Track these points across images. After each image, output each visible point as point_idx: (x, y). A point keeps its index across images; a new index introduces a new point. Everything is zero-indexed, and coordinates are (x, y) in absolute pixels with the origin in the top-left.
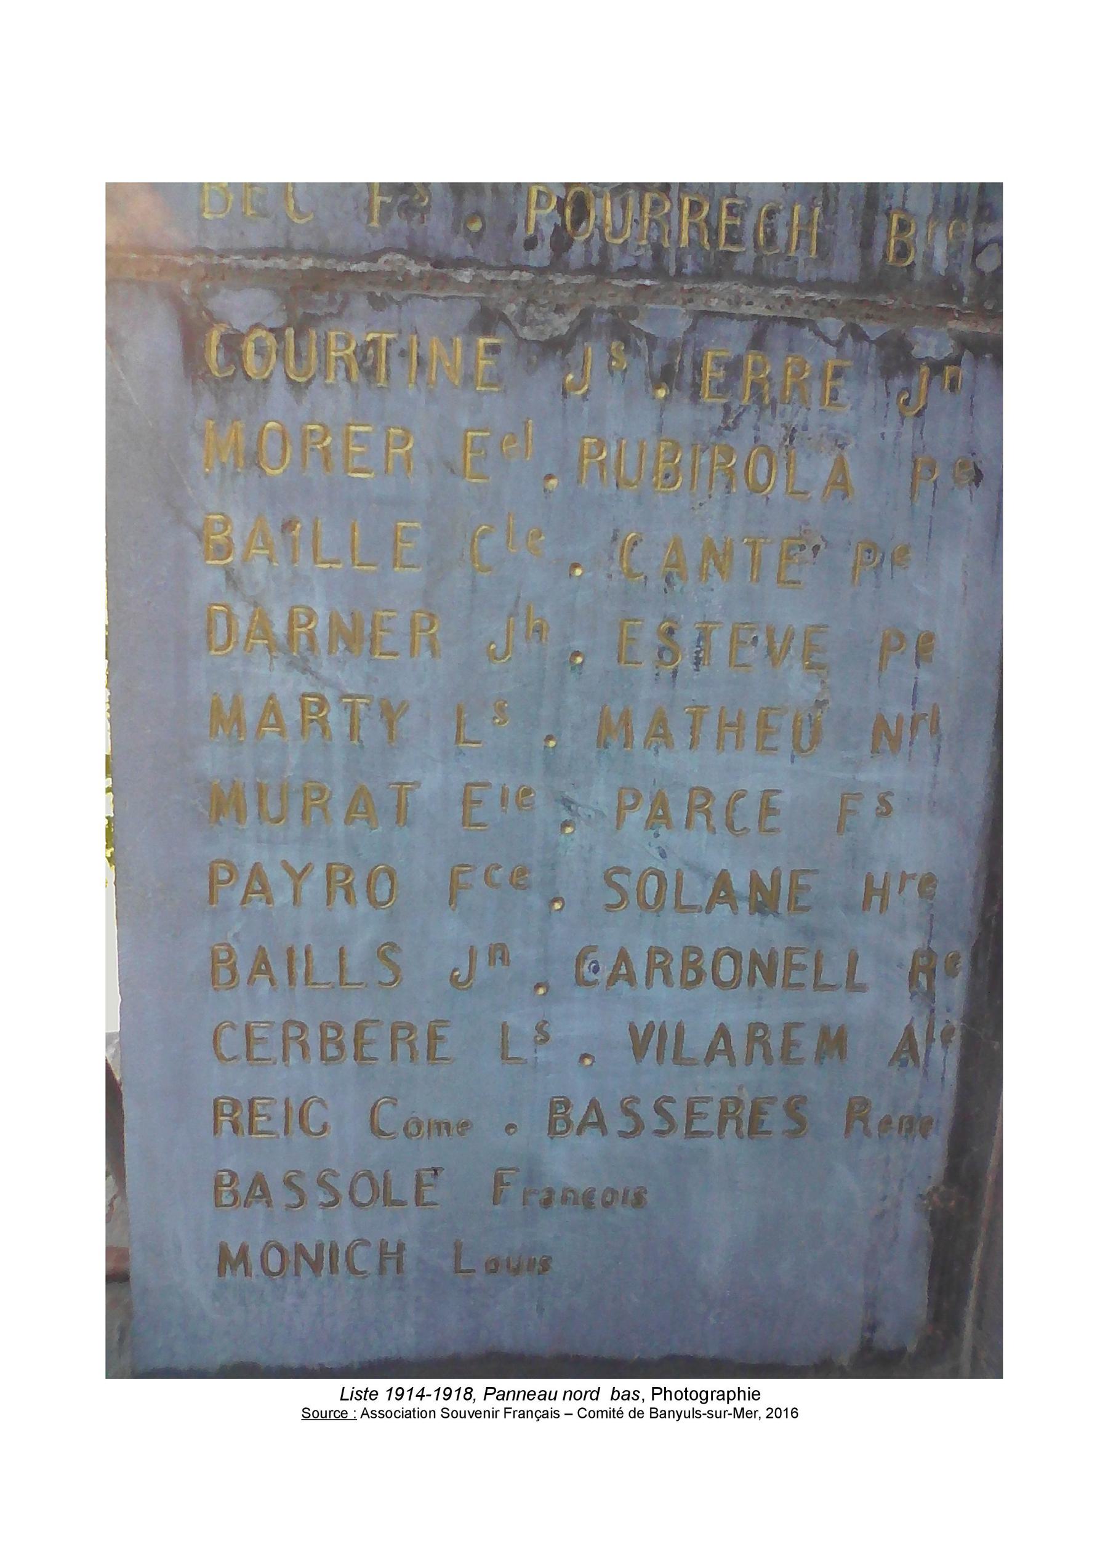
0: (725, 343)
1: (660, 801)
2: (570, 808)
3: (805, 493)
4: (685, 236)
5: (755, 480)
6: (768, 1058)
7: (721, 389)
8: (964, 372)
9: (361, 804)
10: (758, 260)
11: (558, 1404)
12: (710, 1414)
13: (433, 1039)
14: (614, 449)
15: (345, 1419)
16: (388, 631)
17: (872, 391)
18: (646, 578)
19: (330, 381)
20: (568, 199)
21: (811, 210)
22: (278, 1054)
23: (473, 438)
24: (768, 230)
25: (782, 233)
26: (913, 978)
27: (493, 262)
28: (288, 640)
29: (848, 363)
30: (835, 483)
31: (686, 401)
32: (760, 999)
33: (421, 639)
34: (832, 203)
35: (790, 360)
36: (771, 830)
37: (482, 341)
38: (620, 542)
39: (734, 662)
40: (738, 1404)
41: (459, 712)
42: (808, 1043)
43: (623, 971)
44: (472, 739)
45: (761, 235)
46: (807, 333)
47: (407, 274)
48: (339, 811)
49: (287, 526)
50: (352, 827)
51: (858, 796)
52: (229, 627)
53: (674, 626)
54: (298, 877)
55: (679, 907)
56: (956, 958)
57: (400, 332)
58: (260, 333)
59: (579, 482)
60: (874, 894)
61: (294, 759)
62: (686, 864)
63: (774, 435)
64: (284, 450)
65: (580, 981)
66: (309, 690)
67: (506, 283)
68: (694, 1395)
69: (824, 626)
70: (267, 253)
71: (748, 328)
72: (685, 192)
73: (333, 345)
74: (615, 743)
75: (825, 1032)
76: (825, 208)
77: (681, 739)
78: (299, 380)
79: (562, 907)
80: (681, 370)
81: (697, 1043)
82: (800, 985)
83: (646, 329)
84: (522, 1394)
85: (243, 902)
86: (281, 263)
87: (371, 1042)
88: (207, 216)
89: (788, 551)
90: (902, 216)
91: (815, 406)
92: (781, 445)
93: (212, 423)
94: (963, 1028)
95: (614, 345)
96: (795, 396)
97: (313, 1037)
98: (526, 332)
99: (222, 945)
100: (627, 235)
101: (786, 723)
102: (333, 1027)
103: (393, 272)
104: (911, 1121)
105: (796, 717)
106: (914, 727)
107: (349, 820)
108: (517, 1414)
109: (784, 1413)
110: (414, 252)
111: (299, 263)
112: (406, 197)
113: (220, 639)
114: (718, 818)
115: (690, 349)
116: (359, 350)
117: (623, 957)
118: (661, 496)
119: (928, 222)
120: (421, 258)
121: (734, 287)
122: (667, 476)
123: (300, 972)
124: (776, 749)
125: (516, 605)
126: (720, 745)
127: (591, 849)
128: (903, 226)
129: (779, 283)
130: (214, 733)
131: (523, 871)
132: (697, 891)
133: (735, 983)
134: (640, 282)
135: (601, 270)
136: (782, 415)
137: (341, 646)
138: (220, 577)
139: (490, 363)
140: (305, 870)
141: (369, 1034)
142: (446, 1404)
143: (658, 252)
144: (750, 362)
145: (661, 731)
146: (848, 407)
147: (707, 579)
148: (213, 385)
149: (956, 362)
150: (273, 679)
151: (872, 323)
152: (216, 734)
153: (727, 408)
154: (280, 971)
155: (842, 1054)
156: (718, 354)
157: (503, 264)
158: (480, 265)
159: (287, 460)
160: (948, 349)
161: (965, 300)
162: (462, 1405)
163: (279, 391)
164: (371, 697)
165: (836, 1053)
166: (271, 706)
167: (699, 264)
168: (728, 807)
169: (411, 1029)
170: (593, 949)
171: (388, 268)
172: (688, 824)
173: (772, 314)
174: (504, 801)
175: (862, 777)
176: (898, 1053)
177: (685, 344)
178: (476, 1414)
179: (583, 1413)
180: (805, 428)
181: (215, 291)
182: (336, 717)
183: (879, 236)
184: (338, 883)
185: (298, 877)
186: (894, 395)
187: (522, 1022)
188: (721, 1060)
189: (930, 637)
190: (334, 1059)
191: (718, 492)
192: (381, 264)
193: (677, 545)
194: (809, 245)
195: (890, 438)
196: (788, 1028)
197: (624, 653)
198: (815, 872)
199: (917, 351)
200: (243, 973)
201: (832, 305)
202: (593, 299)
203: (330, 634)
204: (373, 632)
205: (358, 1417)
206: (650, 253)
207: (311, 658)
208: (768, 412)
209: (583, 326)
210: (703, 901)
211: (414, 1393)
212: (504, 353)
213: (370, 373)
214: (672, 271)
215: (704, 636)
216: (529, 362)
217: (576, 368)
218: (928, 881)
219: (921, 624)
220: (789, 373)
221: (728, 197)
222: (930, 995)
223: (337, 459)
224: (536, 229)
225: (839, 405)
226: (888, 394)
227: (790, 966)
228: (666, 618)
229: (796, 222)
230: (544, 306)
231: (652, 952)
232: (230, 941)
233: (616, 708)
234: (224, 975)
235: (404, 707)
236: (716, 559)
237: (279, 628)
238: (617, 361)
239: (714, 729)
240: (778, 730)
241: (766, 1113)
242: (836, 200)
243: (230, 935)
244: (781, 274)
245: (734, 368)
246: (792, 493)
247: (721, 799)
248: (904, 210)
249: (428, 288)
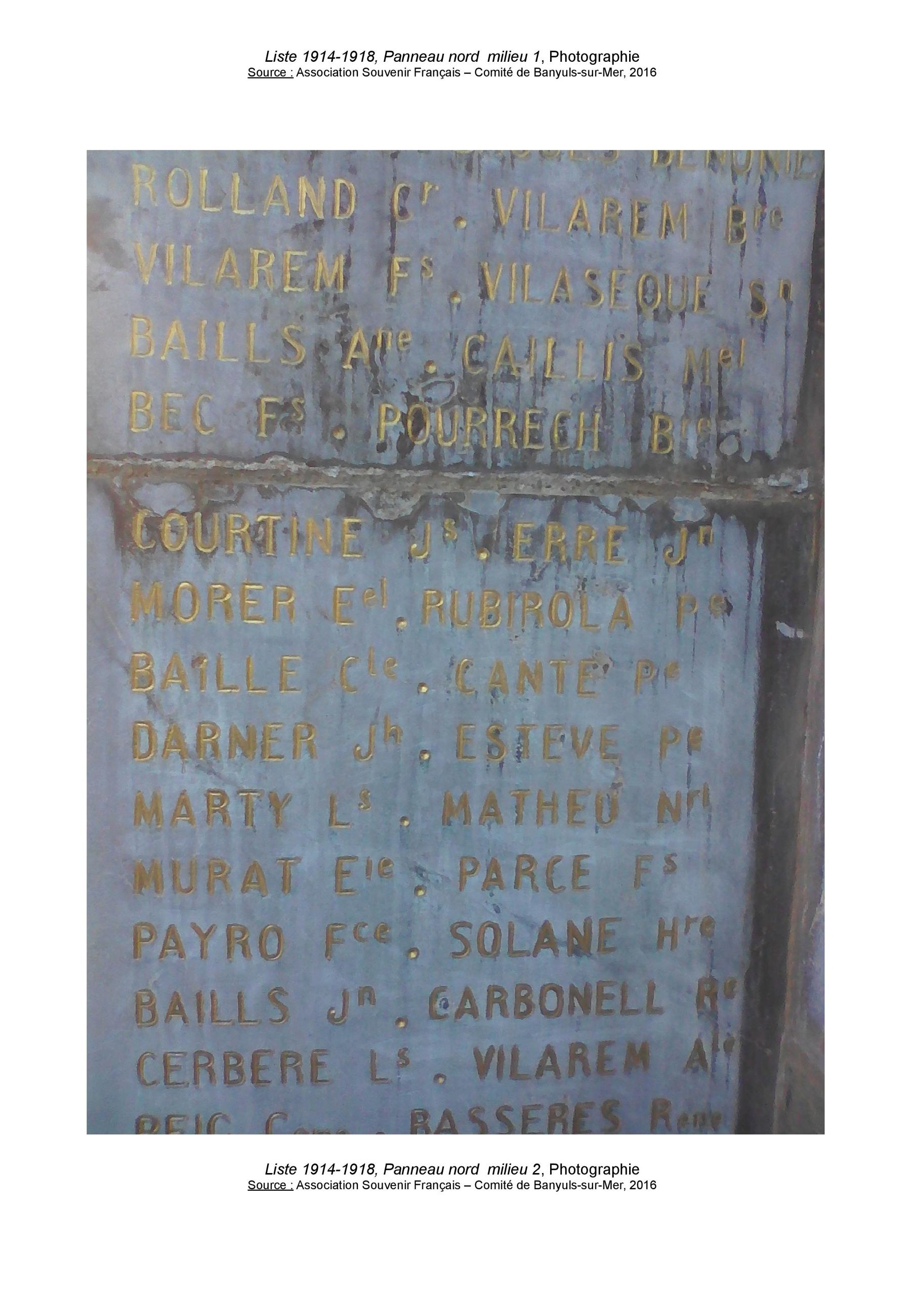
0: (532, 517)
1: (493, 867)
2: (421, 875)
3: (596, 626)
4: (498, 438)
5: (557, 617)
6: (586, 1070)
7: (528, 552)
8: (715, 529)
9: (253, 876)
10: (554, 455)
13: (316, 1064)
14: (449, 598)
15: (283, 1190)
16: (276, 739)
17: (644, 548)
18: (476, 692)
19: (229, 552)
20: (410, 414)
21: (593, 416)
22: (189, 1078)
23: (341, 592)
24: (561, 431)
25: (571, 433)
26: (699, 1002)
27: (354, 462)
28: (197, 751)
29: (624, 528)
30: (619, 618)
31: (503, 561)
32: (579, 1023)
33: (303, 745)
34: (609, 410)
35: (580, 528)
36: (583, 887)
37: (347, 521)
38: (456, 665)
39: (547, 755)
41: (332, 800)
42: (618, 1058)
43: (468, 1006)
44: (343, 821)
45: (556, 435)
46: (592, 507)
47: (288, 471)
48: (236, 880)
49: (197, 661)
50: (247, 895)
51: (649, 858)
52: (150, 739)
53: (499, 728)
54: (204, 936)
55: (512, 953)
56: (732, 984)
57: (284, 515)
58: (175, 516)
59: (423, 622)
60: (667, 934)
61: (201, 841)
62: (516, 916)
63: (570, 584)
64: (194, 604)
65: (434, 1016)
66: (213, 787)
67: (364, 477)
69: (614, 726)
70: (180, 456)
71: (549, 505)
72: (497, 407)
73: (232, 526)
74: (456, 821)
75: (631, 1048)
76: (603, 414)
77: (508, 815)
78: (205, 551)
79: (417, 957)
81: (529, 1061)
82: (610, 1012)
83: (470, 509)
84: (415, 57)
85: (161, 957)
86: (191, 464)
87: (265, 1068)
88: (133, 430)
89: (585, 669)
90: (662, 417)
91: (600, 561)
92: (576, 591)
93: (137, 583)
94: (742, 1040)
95: (447, 521)
96: (585, 554)
97: (218, 1065)
98: (380, 514)
99: (144, 990)
100: (455, 439)
101: (590, 801)
102: (234, 1057)
103: (277, 471)
104: (704, 1117)
105: (597, 797)
106: (690, 801)
107: (244, 890)
108: (425, 1186)
109: (645, 1185)
110: (292, 455)
111: (205, 463)
112: (287, 414)
113: (143, 748)
114: (540, 881)
115: (504, 524)
116: (252, 529)
117: (467, 995)
118: (485, 632)
119: (682, 420)
120: (298, 459)
121: (537, 475)
122: (490, 617)
123: (207, 1011)
124: (583, 822)
125: (376, 715)
126: (539, 819)
127: (439, 908)
128: (663, 425)
129: (570, 470)
130: (137, 822)
131: (385, 928)
132: (526, 939)
133: (557, 1013)
134: (465, 474)
135: (435, 465)
136: (576, 568)
137: (238, 752)
138: (143, 701)
139: (353, 536)
140: (209, 931)
141: (263, 1061)
143: (478, 451)
144: (550, 530)
145: (493, 810)
146: (626, 561)
147: (523, 693)
148: (138, 555)
149: (708, 523)
150: (190, 781)
151: (642, 497)
152: (140, 824)
153: (533, 565)
154: (191, 1012)
155: (646, 1065)
156: (525, 525)
157: (361, 463)
158: (343, 464)
159: (197, 611)
160: (702, 514)
161: (713, 476)
163: (190, 561)
164: (262, 792)
165: (641, 1064)
166: (183, 800)
167: (510, 460)
168: (547, 870)
169: (298, 1057)
170: (443, 989)
171: (273, 467)
172: (517, 885)
173: (565, 495)
174: (368, 871)
175: (651, 842)
176: (690, 1061)
177: (501, 518)
180: (594, 578)
181: (139, 485)
182: (234, 809)
183: (645, 432)
184: (236, 940)
185: (204, 936)
186: (661, 549)
187: (387, 1051)
188: (549, 1074)
189: (698, 731)
190: (235, 1082)
191: (529, 627)
192: (269, 464)
193: (499, 667)
194: (592, 442)
195: (659, 582)
196: (602, 1046)
197: (461, 750)
198: (619, 919)
199: (678, 517)
200: (161, 1012)
201: (611, 485)
202: (430, 488)
203: (230, 743)
204: (264, 739)
205: (294, 1188)
206: (473, 452)
207: (214, 762)
208: (565, 567)
209: (423, 508)
210: (530, 946)
212: (363, 529)
213: (261, 545)
214: (489, 465)
215: (523, 735)
216: (383, 536)
217: (419, 539)
218: (707, 924)
219: (691, 722)
220: (580, 537)
221: (530, 408)
222: (713, 1014)
223: (236, 610)
224: (386, 437)
225: (621, 560)
226: (656, 549)
227: (601, 996)
228: (493, 723)
229: (582, 425)
230: (393, 493)
231: (491, 990)
232: (150, 988)
233: (457, 793)
234: (146, 1015)
235: (288, 798)
236: (530, 676)
237: (190, 739)
238: (450, 532)
239: (534, 808)
240: (584, 807)
241: (587, 1116)
242: (612, 408)
243: (151, 983)
245: (538, 535)
246: (586, 626)
247: (542, 864)
248: (663, 413)
249: (304, 482)
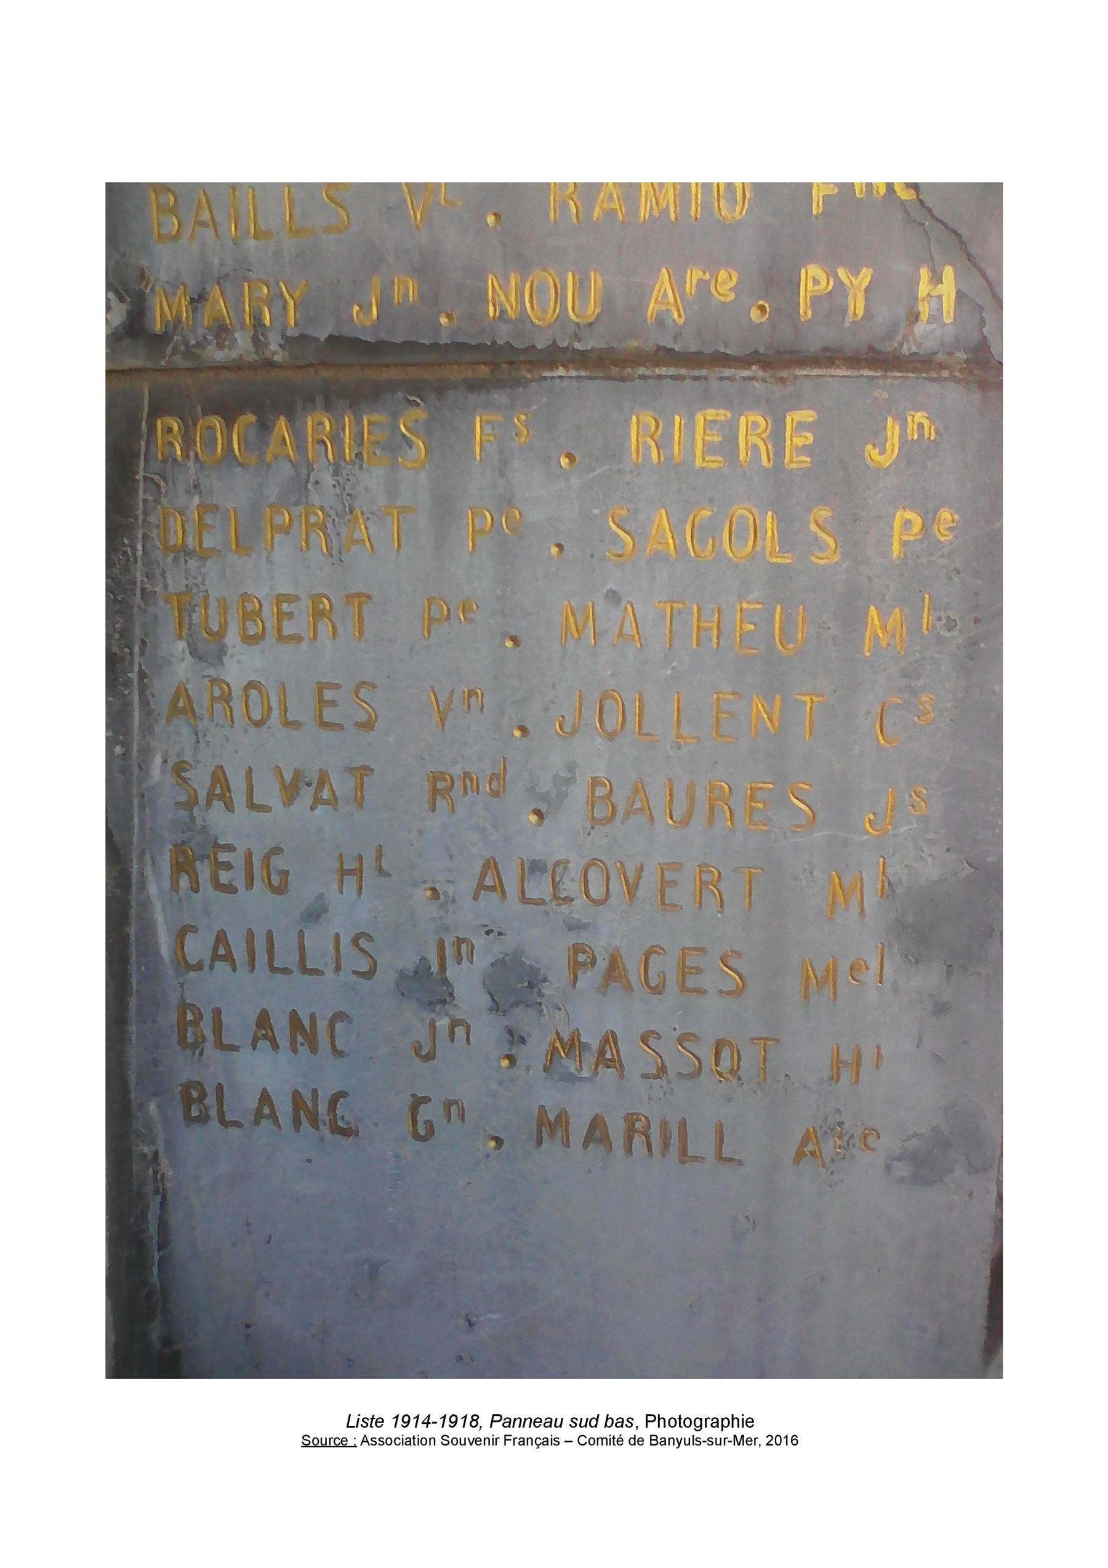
12: (710, 1441)
15: (345, 1446)
40: (739, 1432)
68: (688, 1423)
82: (297, 638)
84: (528, 1421)
108: (517, 1441)
109: (784, 1441)
179: (583, 1440)
205: (358, 1444)
211: (420, 1420)
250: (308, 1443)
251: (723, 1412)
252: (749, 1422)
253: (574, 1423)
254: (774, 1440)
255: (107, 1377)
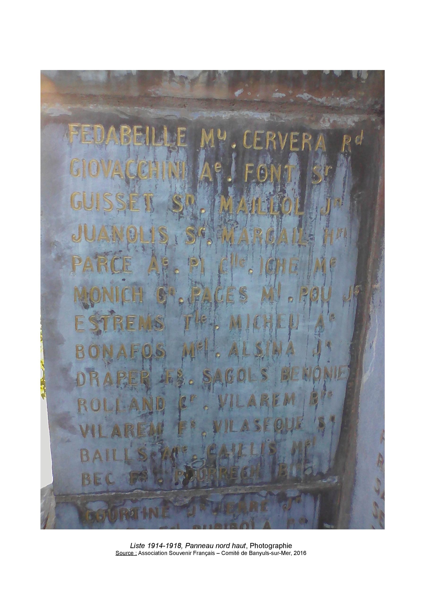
11: (214, 550)
15: (132, 555)
40: (283, 550)
68: (266, 546)
71: (240, 497)
80: (221, 508)
83: (210, 500)
84: (200, 546)
86: (106, 494)
108: (198, 553)
109: (301, 553)
142: (171, 549)
149: (300, 496)
160: (297, 494)
162: (177, 550)
178: (183, 553)
179: (223, 553)
199: (288, 495)
205: (137, 555)
209: (193, 501)
211: (159, 545)
214: (217, 486)
244: (248, 482)
250: (118, 554)
251: (280, 542)
252: (290, 546)
253: (219, 546)
254: (297, 553)
255: (45, 525)
